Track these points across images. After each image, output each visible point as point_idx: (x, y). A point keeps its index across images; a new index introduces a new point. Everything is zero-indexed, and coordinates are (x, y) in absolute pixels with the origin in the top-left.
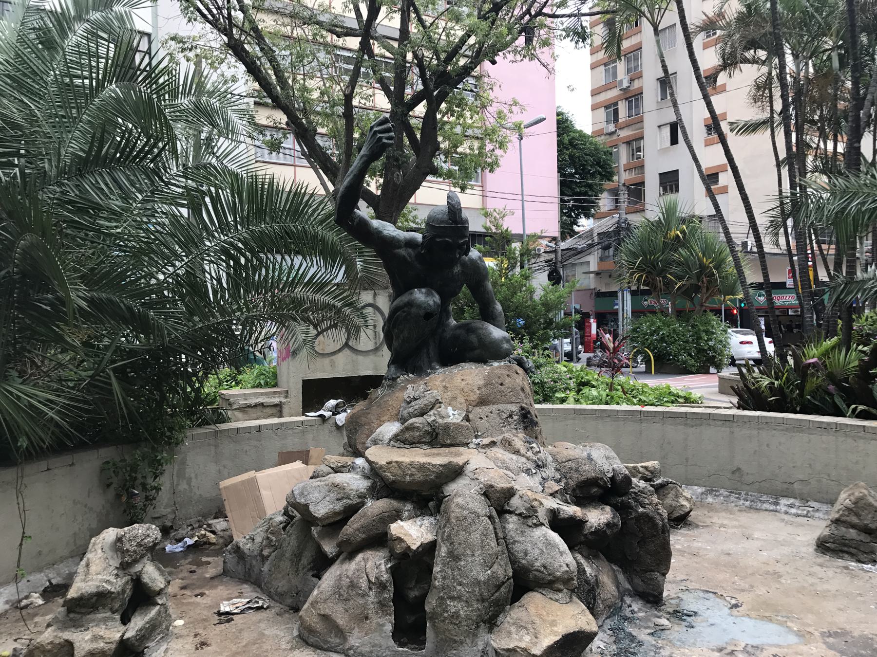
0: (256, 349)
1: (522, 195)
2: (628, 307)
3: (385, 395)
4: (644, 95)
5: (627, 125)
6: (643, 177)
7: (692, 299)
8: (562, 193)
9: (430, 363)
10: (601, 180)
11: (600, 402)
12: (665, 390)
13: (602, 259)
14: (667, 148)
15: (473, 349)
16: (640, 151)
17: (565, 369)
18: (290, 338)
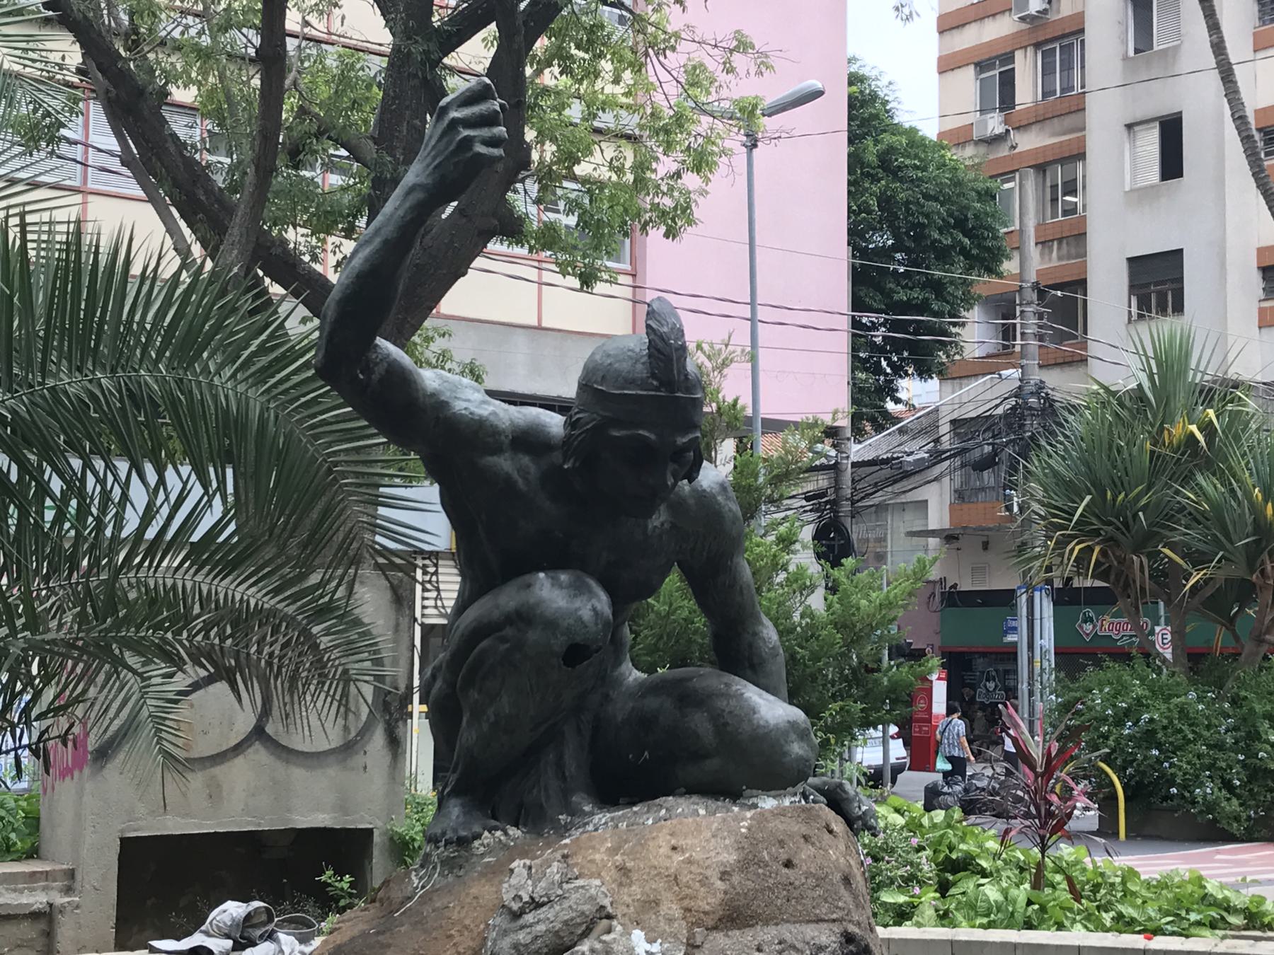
0: (25, 741)
1: (753, 304)
2: (1046, 639)
3: (434, 890)
4: (1089, 36)
5: (1037, 119)
6: (1084, 267)
7: (1232, 620)
8: (858, 304)
9: (566, 794)
10: (968, 270)
11: (1009, 922)
12: (1190, 888)
13: (961, 496)
14: (1152, 187)
15: (699, 756)
16: (1073, 192)
17: (900, 821)
18: (115, 705)
